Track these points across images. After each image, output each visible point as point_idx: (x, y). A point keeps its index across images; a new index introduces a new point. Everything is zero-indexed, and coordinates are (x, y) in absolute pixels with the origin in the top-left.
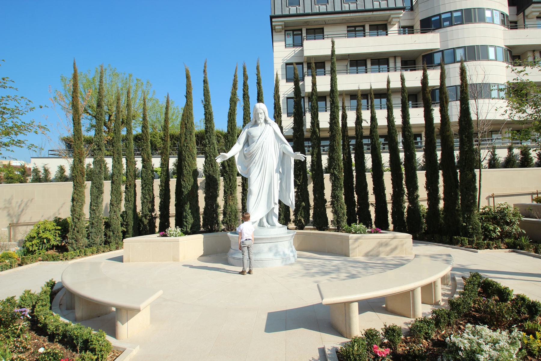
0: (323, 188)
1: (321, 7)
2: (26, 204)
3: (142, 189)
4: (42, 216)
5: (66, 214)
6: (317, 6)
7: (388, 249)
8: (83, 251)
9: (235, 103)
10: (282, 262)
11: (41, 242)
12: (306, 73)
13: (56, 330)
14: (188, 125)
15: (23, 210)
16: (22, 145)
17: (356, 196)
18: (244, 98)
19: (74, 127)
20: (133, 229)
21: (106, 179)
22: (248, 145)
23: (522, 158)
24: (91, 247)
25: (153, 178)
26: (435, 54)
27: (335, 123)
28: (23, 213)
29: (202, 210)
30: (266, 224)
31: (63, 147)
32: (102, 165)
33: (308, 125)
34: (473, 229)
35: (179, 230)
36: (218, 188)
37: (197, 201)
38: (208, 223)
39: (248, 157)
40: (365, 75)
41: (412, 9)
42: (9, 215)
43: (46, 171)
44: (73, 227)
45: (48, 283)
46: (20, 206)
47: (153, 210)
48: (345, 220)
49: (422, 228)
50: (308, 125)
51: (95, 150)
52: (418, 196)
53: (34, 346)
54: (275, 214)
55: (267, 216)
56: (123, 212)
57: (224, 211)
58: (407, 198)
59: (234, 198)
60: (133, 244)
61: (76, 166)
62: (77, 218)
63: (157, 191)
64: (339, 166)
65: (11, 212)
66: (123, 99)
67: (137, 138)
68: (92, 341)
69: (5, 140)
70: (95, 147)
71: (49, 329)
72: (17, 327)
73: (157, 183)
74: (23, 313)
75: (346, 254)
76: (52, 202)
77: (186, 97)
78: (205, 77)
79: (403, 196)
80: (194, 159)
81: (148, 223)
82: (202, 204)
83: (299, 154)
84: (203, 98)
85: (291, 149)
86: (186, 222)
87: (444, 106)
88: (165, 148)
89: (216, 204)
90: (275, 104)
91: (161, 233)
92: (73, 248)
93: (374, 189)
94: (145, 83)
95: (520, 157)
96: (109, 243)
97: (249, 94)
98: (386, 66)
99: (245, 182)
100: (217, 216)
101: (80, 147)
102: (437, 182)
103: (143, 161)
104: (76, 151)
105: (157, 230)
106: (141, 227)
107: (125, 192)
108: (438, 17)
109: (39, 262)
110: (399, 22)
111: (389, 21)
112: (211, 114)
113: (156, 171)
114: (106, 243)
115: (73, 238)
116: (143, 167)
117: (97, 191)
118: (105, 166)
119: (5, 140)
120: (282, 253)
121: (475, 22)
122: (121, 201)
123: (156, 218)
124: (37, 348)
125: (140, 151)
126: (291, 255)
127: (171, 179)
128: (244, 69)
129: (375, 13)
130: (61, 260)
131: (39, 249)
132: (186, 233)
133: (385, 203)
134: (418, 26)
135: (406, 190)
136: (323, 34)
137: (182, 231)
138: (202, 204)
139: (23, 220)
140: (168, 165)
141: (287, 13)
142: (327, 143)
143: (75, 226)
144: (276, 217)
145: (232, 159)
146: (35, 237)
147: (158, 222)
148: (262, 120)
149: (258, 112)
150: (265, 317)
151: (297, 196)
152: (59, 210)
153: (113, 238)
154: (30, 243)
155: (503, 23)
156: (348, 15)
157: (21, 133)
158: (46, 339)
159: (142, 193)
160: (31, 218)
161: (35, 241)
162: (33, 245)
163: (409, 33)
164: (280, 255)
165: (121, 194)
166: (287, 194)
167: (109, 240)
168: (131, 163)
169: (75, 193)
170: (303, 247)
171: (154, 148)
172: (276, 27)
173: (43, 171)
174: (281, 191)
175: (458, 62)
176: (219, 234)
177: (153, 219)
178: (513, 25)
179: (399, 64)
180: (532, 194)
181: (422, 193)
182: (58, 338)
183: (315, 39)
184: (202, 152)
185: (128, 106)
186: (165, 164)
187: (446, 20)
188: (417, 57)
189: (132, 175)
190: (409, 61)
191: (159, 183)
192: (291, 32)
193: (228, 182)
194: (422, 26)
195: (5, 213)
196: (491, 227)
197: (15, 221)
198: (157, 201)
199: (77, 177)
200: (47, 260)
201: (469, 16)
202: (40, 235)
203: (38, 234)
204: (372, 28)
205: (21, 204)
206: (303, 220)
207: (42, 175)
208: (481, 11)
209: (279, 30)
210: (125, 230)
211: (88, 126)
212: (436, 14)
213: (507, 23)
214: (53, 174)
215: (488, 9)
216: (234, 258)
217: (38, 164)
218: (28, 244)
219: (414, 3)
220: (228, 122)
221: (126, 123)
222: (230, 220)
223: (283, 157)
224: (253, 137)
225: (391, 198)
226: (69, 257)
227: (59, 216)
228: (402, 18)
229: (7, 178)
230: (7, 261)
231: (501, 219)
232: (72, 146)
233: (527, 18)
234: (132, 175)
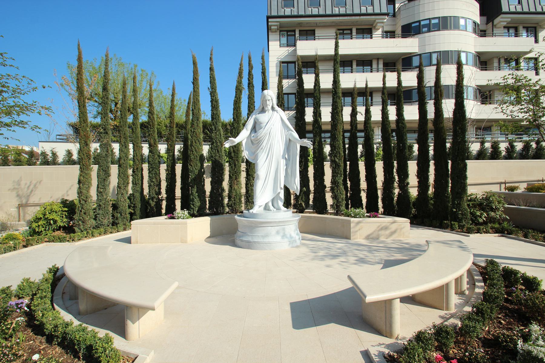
0: (323, 174)
2: (35, 185)
3: (149, 173)
4: (51, 197)
5: (72, 196)
7: (388, 232)
8: (91, 232)
9: (241, 92)
10: (289, 244)
11: (47, 223)
13: (55, 331)
14: (195, 111)
15: (32, 191)
16: (25, 126)
18: (248, 86)
19: (79, 109)
20: (141, 211)
21: (113, 163)
22: (256, 132)
23: (492, 151)
24: (99, 228)
25: (160, 163)
26: (413, 58)
27: (337, 112)
28: (32, 194)
29: (208, 194)
30: (272, 208)
31: (71, 131)
32: (109, 148)
34: (462, 214)
35: (186, 212)
36: (223, 173)
38: (215, 207)
40: (351, 74)
41: (394, 15)
43: (54, 154)
44: (80, 209)
45: (50, 269)
46: (28, 187)
47: (159, 193)
48: (344, 205)
49: (411, 212)
51: (101, 133)
52: (408, 184)
53: (28, 350)
54: (280, 199)
55: (273, 201)
56: (131, 194)
57: (229, 194)
58: (397, 185)
59: (239, 183)
60: (141, 226)
61: (82, 149)
62: (83, 200)
63: (163, 175)
64: (340, 154)
65: (20, 193)
66: (129, 88)
67: (143, 125)
68: (97, 349)
69: (6, 120)
70: (101, 132)
71: (47, 329)
72: (9, 326)
73: (163, 168)
74: (19, 306)
75: (348, 237)
76: (59, 185)
77: (193, 83)
78: (211, 65)
79: (394, 183)
80: (201, 145)
81: (155, 205)
82: (208, 188)
84: (209, 85)
85: (296, 135)
86: (193, 205)
87: (438, 99)
88: (171, 134)
89: (221, 188)
91: (169, 215)
92: (80, 229)
93: (366, 176)
94: (149, 74)
95: (490, 150)
96: (117, 224)
97: (254, 83)
98: (370, 67)
99: (251, 167)
100: (223, 199)
101: (86, 130)
102: (428, 171)
103: (150, 145)
104: (82, 133)
105: (164, 211)
106: (149, 210)
107: (133, 176)
108: (418, 24)
109: (45, 244)
110: (383, 27)
111: (374, 25)
112: (217, 101)
113: (162, 157)
114: (114, 224)
115: (80, 220)
116: (150, 152)
117: (137, 172)
118: (112, 151)
119: (6, 120)
120: (288, 236)
121: (451, 29)
122: (128, 183)
123: (162, 200)
124: (31, 353)
125: (146, 137)
126: (297, 237)
127: (177, 165)
129: (362, 17)
130: (68, 241)
131: (45, 230)
132: (193, 215)
133: (376, 189)
134: (399, 31)
135: (397, 178)
136: (314, 35)
137: (189, 213)
138: (208, 188)
139: (32, 201)
140: (174, 150)
141: (283, 14)
142: (362, 134)
143: (82, 208)
144: (281, 201)
145: (239, 144)
146: (41, 218)
147: (164, 204)
148: (270, 107)
149: (266, 98)
150: (288, 308)
152: (67, 192)
153: (120, 219)
154: (37, 224)
155: (475, 32)
156: (338, 18)
157: (23, 113)
158: (44, 339)
159: (149, 176)
160: (40, 199)
161: (41, 223)
162: (39, 226)
163: (390, 38)
164: (287, 237)
165: (128, 177)
166: (293, 179)
167: (117, 221)
168: (138, 149)
169: (81, 175)
170: (305, 229)
171: (160, 136)
172: (272, 28)
173: (51, 155)
174: (286, 176)
175: (434, 65)
176: (225, 216)
177: (159, 201)
178: (483, 34)
179: (381, 66)
180: (500, 183)
181: (413, 180)
182: (57, 341)
183: (307, 40)
184: (208, 139)
185: (134, 91)
186: (171, 150)
187: (424, 26)
188: (397, 60)
189: (139, 159)
190: (391, 63)
191: (166, 168)
192: (286, 33)
193: (233, 167)
195: (14, 193)
196: (478, 213)
197: (24, 202)
198: (164, 185)
199: (83, 161)
200: (53, 241)
201: (445, 23)
202: (46, 217)
203: (45, 215)
205: (30, 185)
206: (303, 204)
207: (50, 157)
208: (456, 19)
209: (274, 30)
210: (133, 211)
211: (95, 113)
212: (416, 20)
214: (61, 157)
215: (463, 18)
216: (242, 241)
217: (47, 148)
218: (34, 225)
219: (396, 10)
220: (234, 109)
221: (134, 110)
222: (234, 203)
223: (289, 143)
224: (261, 123)
225: (382, 185)
226: (76, 239)
227: (66, 198)
228: (385, 24)
229: (15, 161)
230: (11, 242)
231: (486, 205)
232: (79, 131)
234: (139, 159)
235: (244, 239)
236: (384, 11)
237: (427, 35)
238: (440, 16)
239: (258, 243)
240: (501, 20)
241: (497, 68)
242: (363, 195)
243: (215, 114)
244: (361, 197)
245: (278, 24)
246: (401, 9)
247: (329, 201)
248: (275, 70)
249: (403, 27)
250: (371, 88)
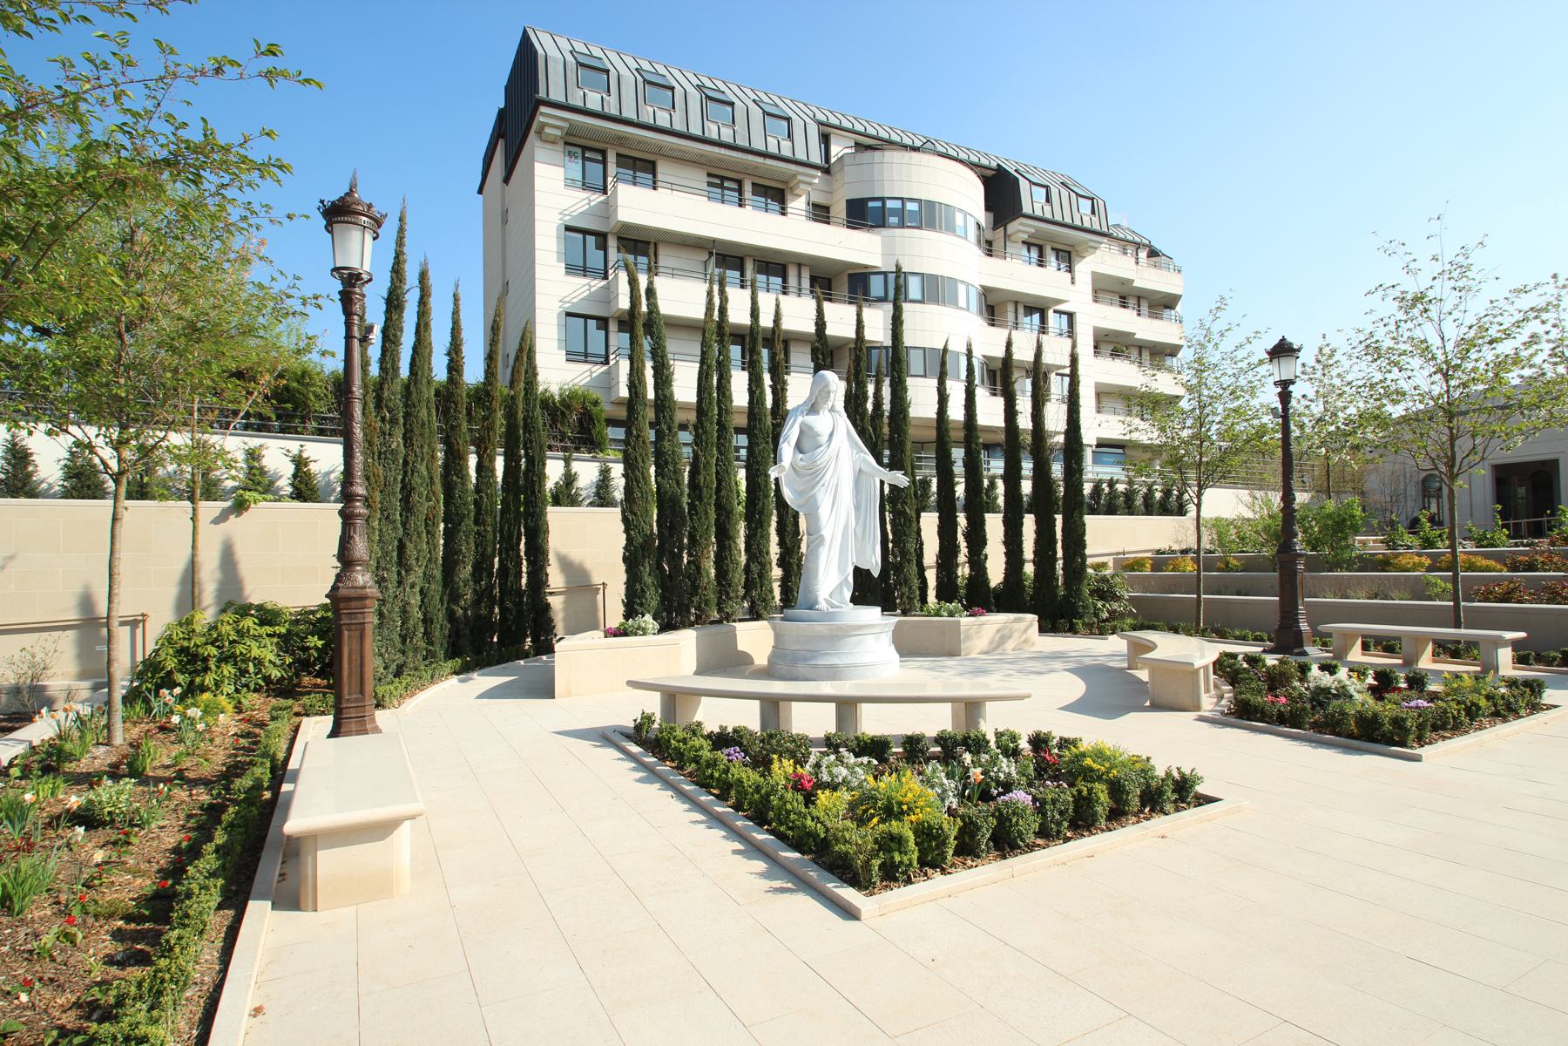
6: (650, 110)
37: (1037, 532)
108: (879, 204)
112: (427, 325)
129: (769, 162)
134: (839, 210)
179: (806, 283)
187: (894, 212)
188: (840, 273)
190: (829, 280)
192: (579, 150)
204: (760, 190)
216: (816, 666)
219: (833, 160)
223: (859, 475)
235: (821, 662)
237: (898, 232)
240: (1018, 227)
243: (455, 367)
246: (847, 161)
248: (554, 247)
249: (849, 202)
250: (787, 332)
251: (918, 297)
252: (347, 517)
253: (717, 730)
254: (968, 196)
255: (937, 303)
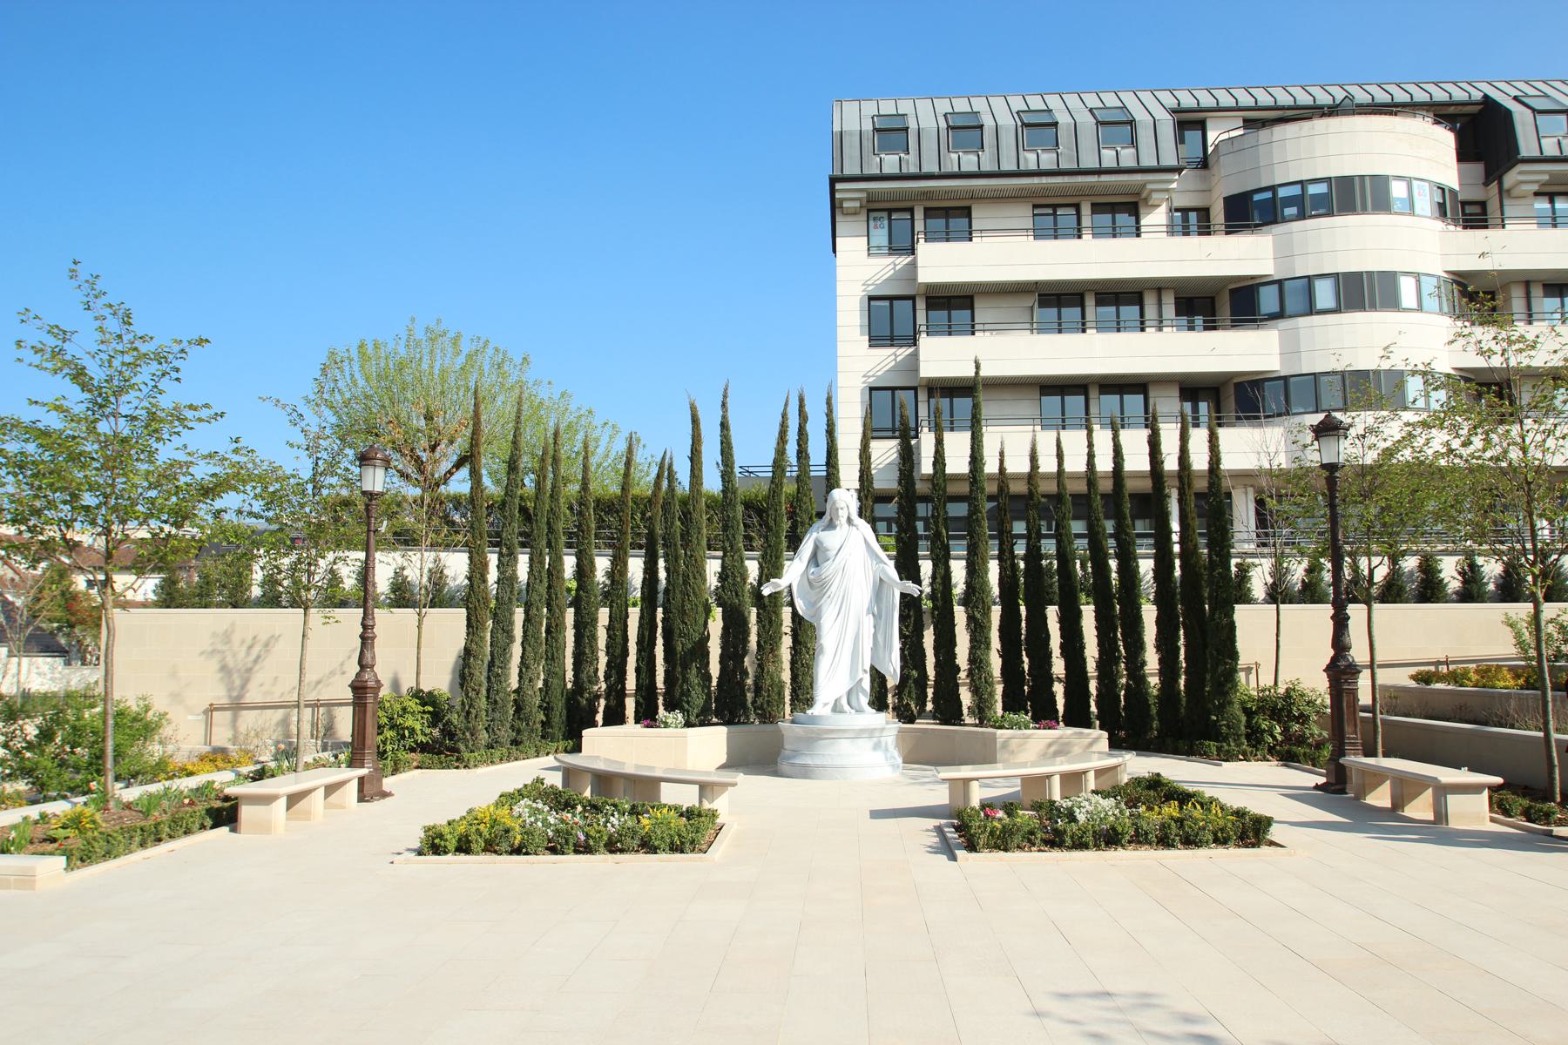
1: (964, 158)
12: (923, 328)
15: (258, 657)
17: (1026, 659)
33: (927, 467)
34: (1228, 727)
39: (817, 586)
42: (224, 668)
46: (250, 647)
50: (927, 467)
54: (863, 691)
55: (849, 693)
57: (756, 683)
59: (777, 659)
65: (230, 661)
79: (1117, 664)
83: (910, 584)
85: (894, 574)
90: (861, 471)
93: (1062, 646)
97: (810, 450)
99: (804, 632)
108: (1268, 195)
111: (1144, 195)
121: (1364, 210)
123: (598, 697)
128: (801, 400)
129: (1104, 178)
134: (1218, 215)
139: (253, 696)
148: (844, 520)
151: (903, 657)
156: (1036, 180)
174: (875, 649)
178: (1472, 214)
179: (1169, 310)
181: (1152, 659)
187: (1289, 201)
190: (1203, 303)
192: (885, 214)
194: (1229, 215)
195: (214, 664)
212: (1264, 185)
213: (1454, 210)
219: (1210, 150)
223: (880, 586)
233: (1509, 196)
236: (1169, 160)
238: (1332, 175)
239: (823, 767)
241: (1524, 317)
242: (1059, 689)
244: (1052, 696)
245: (864, 195)
246: (1222, 150)
247: (966, 697)
248: (857, 321)
249: (1228, 200)
251: (1331, 304)
252: (473, 625)
253: (134, 706)
254: (1427, 156)
255: (1362, 308)
